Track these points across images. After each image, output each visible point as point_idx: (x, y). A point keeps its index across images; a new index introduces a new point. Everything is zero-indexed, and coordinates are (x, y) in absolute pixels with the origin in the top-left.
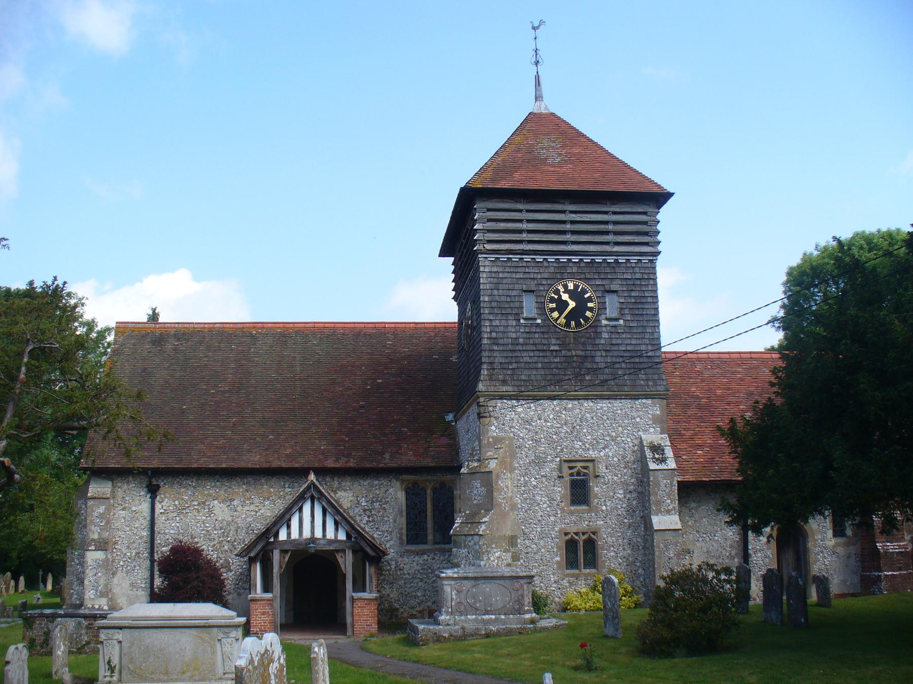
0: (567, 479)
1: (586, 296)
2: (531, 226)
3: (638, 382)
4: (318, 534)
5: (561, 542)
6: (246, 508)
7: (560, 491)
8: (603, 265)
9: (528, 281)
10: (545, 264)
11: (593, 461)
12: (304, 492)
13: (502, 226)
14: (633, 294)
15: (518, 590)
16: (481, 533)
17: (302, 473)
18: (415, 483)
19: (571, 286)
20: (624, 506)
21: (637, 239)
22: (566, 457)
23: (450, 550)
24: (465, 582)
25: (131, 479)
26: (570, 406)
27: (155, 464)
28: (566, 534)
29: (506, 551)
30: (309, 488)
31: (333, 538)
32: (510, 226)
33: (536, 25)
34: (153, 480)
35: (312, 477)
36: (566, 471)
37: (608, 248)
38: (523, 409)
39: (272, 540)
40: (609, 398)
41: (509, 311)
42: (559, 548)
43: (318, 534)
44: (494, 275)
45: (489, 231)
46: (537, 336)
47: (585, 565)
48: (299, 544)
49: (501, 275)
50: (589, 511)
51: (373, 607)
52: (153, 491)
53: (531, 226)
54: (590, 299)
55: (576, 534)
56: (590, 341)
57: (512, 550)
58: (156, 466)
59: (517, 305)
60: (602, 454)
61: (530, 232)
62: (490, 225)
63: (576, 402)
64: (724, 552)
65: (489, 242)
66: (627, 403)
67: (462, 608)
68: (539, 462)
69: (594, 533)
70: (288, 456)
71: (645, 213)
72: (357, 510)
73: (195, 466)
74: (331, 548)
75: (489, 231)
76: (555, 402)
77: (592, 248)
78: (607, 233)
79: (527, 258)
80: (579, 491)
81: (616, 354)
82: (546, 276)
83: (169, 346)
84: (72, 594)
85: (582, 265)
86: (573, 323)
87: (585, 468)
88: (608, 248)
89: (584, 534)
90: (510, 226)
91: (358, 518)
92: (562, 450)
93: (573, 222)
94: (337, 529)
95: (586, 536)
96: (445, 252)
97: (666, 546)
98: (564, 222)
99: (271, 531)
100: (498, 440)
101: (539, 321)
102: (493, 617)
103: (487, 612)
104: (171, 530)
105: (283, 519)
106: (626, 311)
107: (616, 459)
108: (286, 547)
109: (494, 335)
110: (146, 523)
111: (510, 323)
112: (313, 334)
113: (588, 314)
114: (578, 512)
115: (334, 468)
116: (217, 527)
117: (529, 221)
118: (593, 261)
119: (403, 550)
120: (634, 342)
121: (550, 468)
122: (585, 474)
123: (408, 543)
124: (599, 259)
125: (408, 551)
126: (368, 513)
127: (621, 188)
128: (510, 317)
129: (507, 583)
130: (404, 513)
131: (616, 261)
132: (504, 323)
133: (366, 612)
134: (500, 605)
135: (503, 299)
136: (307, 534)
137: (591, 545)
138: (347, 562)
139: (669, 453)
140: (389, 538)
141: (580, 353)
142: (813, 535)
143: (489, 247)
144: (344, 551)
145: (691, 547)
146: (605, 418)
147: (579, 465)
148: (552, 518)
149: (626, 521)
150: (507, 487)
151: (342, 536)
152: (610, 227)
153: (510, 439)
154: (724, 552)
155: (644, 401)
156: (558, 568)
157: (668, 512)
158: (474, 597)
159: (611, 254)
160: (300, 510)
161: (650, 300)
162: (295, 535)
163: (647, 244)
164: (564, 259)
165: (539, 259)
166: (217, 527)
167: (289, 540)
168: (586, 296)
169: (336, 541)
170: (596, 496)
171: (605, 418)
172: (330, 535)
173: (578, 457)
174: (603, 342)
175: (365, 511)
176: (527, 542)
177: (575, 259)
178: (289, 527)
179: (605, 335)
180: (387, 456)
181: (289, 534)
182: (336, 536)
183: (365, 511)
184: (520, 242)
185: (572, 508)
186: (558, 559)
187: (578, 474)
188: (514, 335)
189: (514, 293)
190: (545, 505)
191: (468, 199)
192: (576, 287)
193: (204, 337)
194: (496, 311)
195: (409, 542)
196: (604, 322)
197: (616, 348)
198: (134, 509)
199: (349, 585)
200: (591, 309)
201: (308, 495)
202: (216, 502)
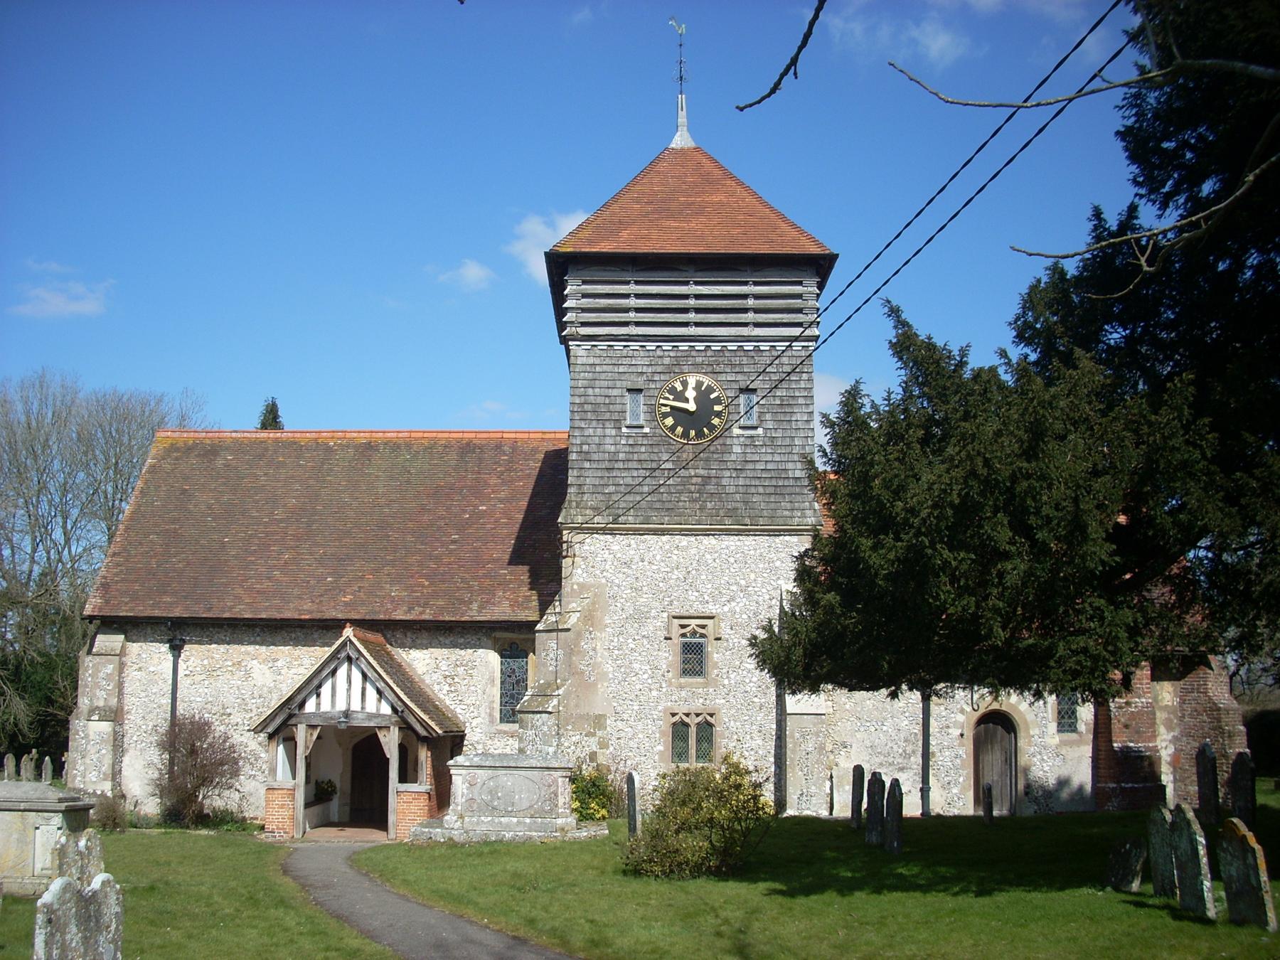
0: (677, 641)
1: (712, 396)
2: (642, 303)
3: (779, 513)
5: (665, 725)
6: (293, 671)
7: (668, 656)
9: (633, 377)
11: (712, 618)
12: (338, 651)
15: (550, 786)
16: (550, 709)
17: (334, 626)
20: (755, 679)
22: (677, 612)
24: (480, 772)
25: (149, 631)
27: (177, 612)
28: (673, 715)
30: (344, 645)
31: (374, 711)
34: (177, 632)
35: (348, 632)
36: (676, 632)
38: (617, 544)
41: (607, 416)
42: (662, 733)
43: (356, 705)
44: (588, 368)
45: (584, 310)
46: (643, 449)
47: (698, 757)
48: (331, 718)
49: (598, 369)
50: (706, 685)
52: (176, 649)
53: (642, 303)
54: (718, 401)
55: (687, 715)
56: (715, 456)
57: (599, 733)
58: (178, 615)
59: (618, 408)
60: (726, 609)
61: (638, 310)
62: (586, 302)
63: (693, 539)
64: (895, 747)
65: (584, 324)
66: (764, 541)
67: (475, 807)
68: (640, 617)
69: (711, 715)
70: (346, 604)
71: (800, 283)
72: (435, 676)
73: (227, 615)
74: (372, 724)
75: (584, 310)
78: (745, 310)
80: (693, 657)
81: (750, 474)
82: (659, 369)
83: (220, 462)
84: (75, 776)
86: (693, 433)
87: (703, 627)
88: (693, 331)
89: (698, 715)
91: (436, 688)
92: (671, 603)
95: (700, 719)
97: (803, 736)
98: (686, 297)
100: (583, 587)
101: (647, 430)
102: (515, 820)
103: (508, 814)
104: (193, 702)
105: (312, 685)
106: (768, 417)
107: (745, 616)
109: (585, 448)
110: (168, 688)
111: (608, 432)
112: (409, 446)
113: (716, 421)
114: (690, 685)
116: (256, 695)
117: (638, 296)
120: (777, 458)
121: (656, 625)
122: (703, 636)
123: (502, 721)
125: (500, 732)
126: (449, 680)
127: (765, 249)
128: (607, 424)
129: (535, 774)
132: (599, 432)
133: (413, 808)
134: (525, 804)
135: (600, 400)
136: (341, 706)
137: (706, 730)
138: (390, 742)
140: (476, 714)
141: (702, 472)
142: (1027, 729)
145: (849, 740)
146: (732, 560)
147: (694, 622)
148: (655, 693)
149: (756, 700)
150: (594, 649)
151: (386, 709)
152: (751, 302)
153: (600, 586)
154: (895, 747)
155: (787, 538)
156: (661, 760)
158: (490, 792)
159: (748, 339)
160: (334, 672)
161: (801, 401)
162: (326, 706)
164: (684, 346)
166: (256, 695)
168: (712, 396)
169: (378, 715)
170: (716, 666)
171: (732, 560)
173: (692, 612)
174: (733, 457)
177: (700, 346)
178: (318, 695)
179: (737, 449)
180: (475, 606)
181: (318, 705)
182: (378, 709)
184: (626, 324)
185: (682, 680)
186: (661, 748)
187: (694, 633)
188: (612, 449)
189: (615, 392)
190: (646, 676)
193: (266, 449)
194: (589, 415)
196: (736, 431)
197: (750, 466)
198: (152, 669)
200: (719, 414)
201: (343, 655)
202: (255, 662)
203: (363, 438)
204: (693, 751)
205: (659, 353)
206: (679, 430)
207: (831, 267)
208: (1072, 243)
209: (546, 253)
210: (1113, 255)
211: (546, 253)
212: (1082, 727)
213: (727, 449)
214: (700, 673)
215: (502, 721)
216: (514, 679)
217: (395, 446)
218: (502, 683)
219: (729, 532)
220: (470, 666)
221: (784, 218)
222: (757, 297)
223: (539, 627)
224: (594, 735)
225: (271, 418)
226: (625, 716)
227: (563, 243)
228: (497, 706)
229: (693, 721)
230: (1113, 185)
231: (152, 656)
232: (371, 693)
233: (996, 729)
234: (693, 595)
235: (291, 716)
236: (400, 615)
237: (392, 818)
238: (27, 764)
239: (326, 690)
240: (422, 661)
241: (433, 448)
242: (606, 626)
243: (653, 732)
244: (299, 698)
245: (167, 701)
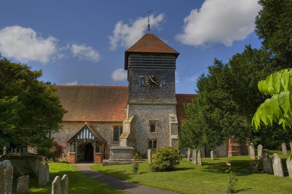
2: (154, 64)
4: (87, 138)
5: (148, 141)
6: (73, 131)
8: (161, 71)
10: (146, 71)
13: (136, 61)
14: (169, 79)
18: (116, 126)
19: (152, 77)
21: (170, 65)
23: (119, 143)
26: (151, 107)
29: (133, 143)
30: (85, 126)
32: (137, 61)
33: (149, 11)
35: (86, 123)
39: (75, 139)
43: (87, 138)
53: (154, 64)
55: (152, 139)
76: (147, 106)
77: (158, 67)
78: (162, 63)
79: (142, 69)
85: (156, 71)
86: (153, 86)
88: (153, 67)
89: (154, 139)
90: (137, 61)
91: (101, 134)
93: (142, 60)
94: (92, 136)
99: (75, 136)
102: (123, 160)
105: (79, 133)
108: (79, 141)
115: (95, 122)
118: (158, 70)
119: (112, 142)
124: (160, 70)
125: (113, 143)
130: (113, 133)
136: (194, 151)
139: (176, 119)
144: (93, 142)
147: (153, 122)
148: (146, 135)
151: (93, 138)
152: (163, 62)
157: (175, 134)
162: (81, 138)
163: (172, 66)
164: (151, 70)
165: (145, 70)
167: (80, 139)
169: (92, 139)
172: (90, 138)
175: (103, 132)
176: (139, 141)
177: (154, 70)
178: (80, 136)
181: (80, 137)
182: (92, 138)
183: (103, 132)
186: (147, 145)
187: (153, 124)
192: (154, 77)
195: (114, 140)
199: (95, 151)
204: (153, 146)
205: (146, 71)
206: (150, 85)
207: (178, 56)
209: (125, 52)
211: (125, 52)
215: (114, 141)
216: (116, 133)
218: (114, 133)
222: (164, 61)
223: (123, 122)
224: (134, 143)
226: (140, 139)
227: (128, 50)
228: (113, 138)
229: (153, 141)
238: (16, 150)
242: (137, 122)
243: (146, 142)
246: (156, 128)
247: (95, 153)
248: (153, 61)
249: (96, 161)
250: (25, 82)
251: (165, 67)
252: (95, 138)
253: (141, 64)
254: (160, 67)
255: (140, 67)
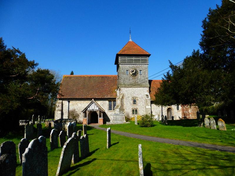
7: (132, 102)
27: (69, 98)
34: (69, 100)
35: (93, 100)
37: (140, 63)
38: (126, 89)
40: (140, 87)
43: (94, 109)
51: (102, 120)
52: (69, 102)
53: (142, 62)
68: (129, 97)
77: (138, 63)
80: (135, 102)
83: (72, 79)
88: (140, 63)
96: (115, 64)
99: (86, 109)
104: (71, 108)
105: (89, 106)
112: (95, 77)
121: (131, 98)
129: (121, 116)
131: (141, 66)
136: (92, 109)
137: (136, 111)
138: (98, 113)
139: (149, 96)
143: (121, 63)
151: (98, 109)
152: (141, 60)
160: (91, 105)
162: (90, 108)
172: (96, 109)
180: (106, 96)
191: (118, 56)
199: (99, 116)
203: (89, 76)
204: (135, 113)
208: (190, 54)
210: (196, 55)
212: (179, 109)
213: (138, 77)
214: (135, 104)
217: (93, 77)
219: (139, 87)
220: (105, 103)
221: (144, 50)
225: (72, 73)
230: (197, 48)
231: (66, 103)
232: (96, 106)
233: (169, 110)
234: (135, 95)
235: (86, 110)
236: (97, 97)
237: (99, 122)
239: (90, 107)
240: (99, 102)
241: (98, 77)
244: (87, 108)
245: (68, 109)
246: (137, 102)
247: (99, 118)
248: (134, 59)
249: (146, 163)
250: (134, 122)
251: (141, 63)
252: (99, 109)
253: (134, 60)
254: (139, 63)
255: (126, 63)
